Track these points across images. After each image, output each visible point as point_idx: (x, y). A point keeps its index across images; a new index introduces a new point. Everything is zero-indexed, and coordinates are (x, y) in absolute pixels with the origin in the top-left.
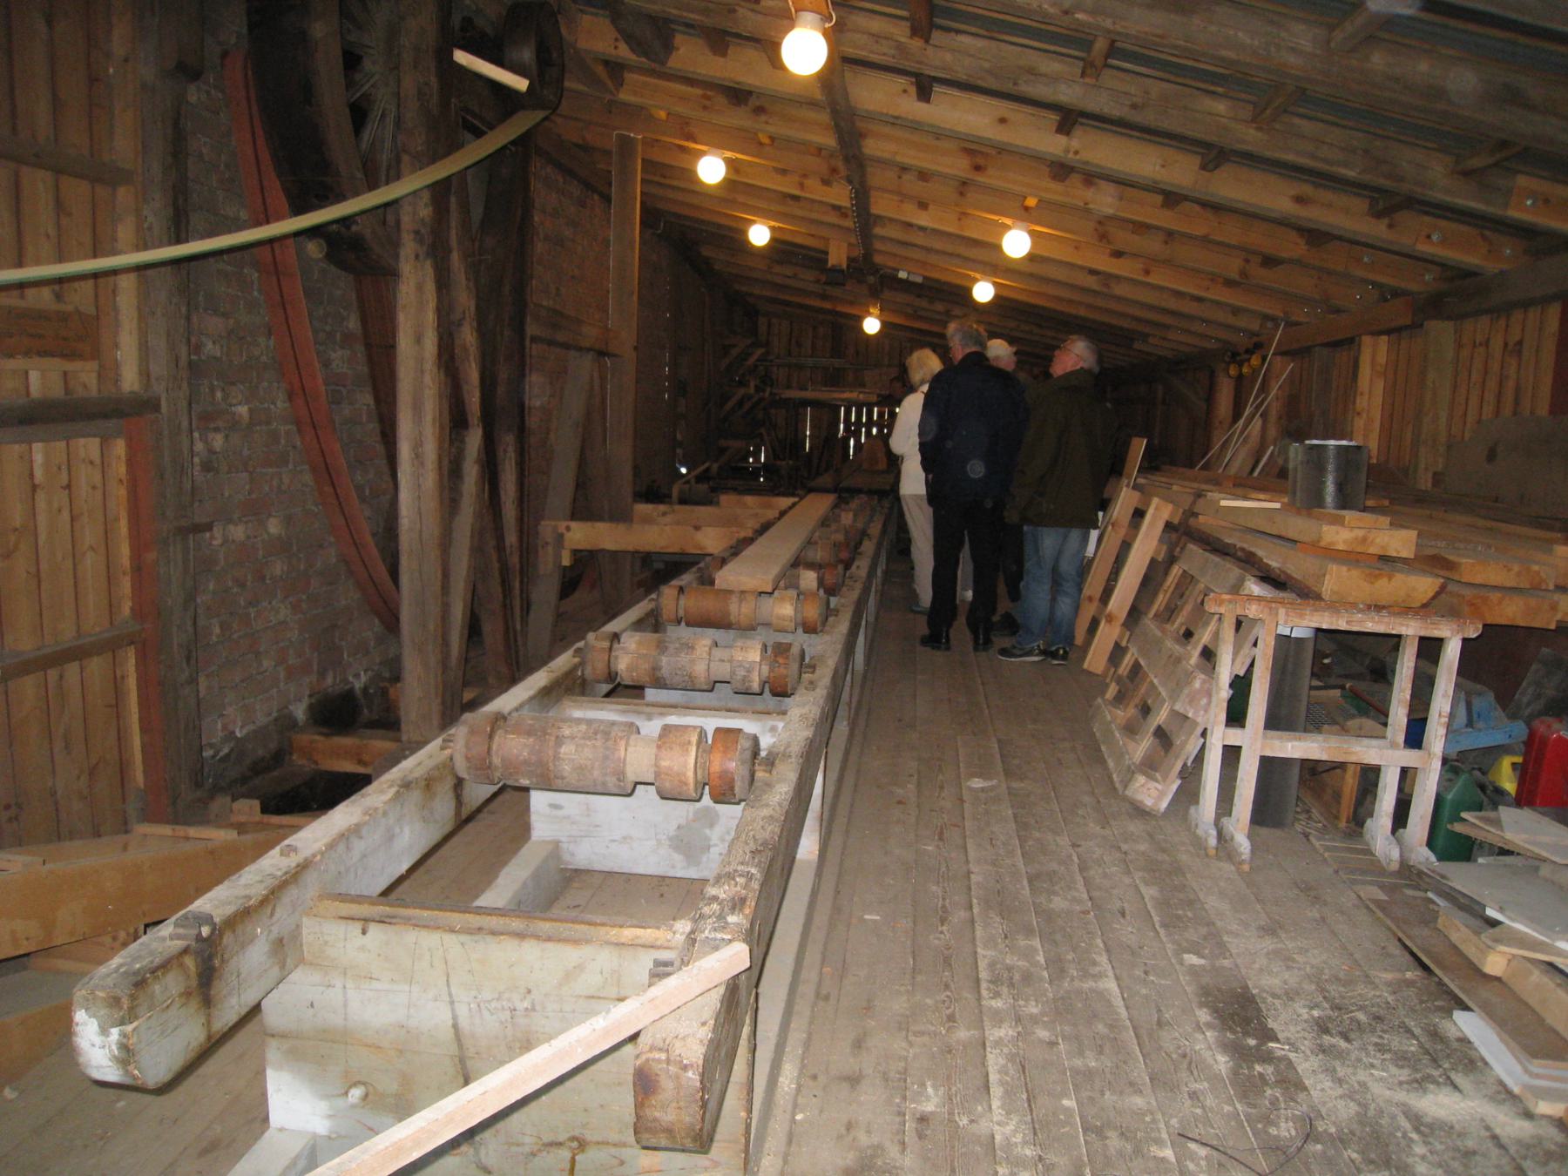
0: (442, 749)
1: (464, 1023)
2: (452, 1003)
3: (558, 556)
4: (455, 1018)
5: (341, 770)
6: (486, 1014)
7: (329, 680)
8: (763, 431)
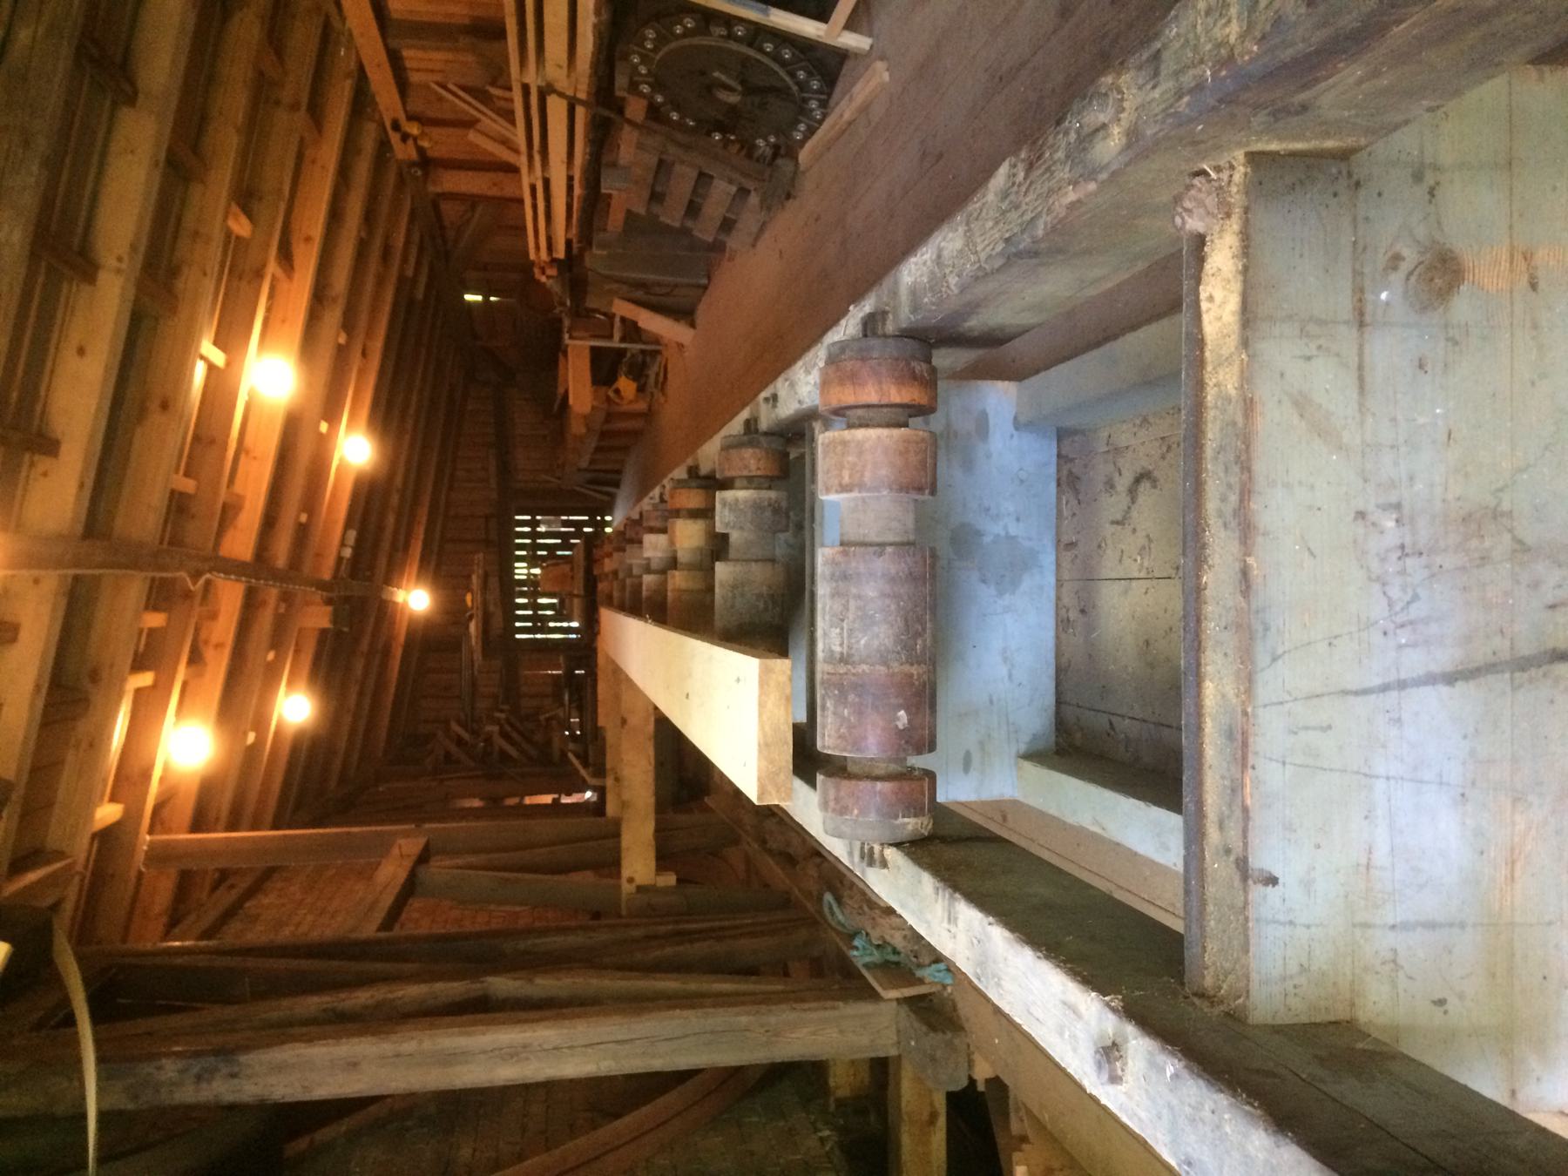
0: (884, 864)
1: (1445, 658)
2: (1402, 685)
3: (666, 891)
4: (1431, 679)
6: (1416, 611)
8: (542, 718)
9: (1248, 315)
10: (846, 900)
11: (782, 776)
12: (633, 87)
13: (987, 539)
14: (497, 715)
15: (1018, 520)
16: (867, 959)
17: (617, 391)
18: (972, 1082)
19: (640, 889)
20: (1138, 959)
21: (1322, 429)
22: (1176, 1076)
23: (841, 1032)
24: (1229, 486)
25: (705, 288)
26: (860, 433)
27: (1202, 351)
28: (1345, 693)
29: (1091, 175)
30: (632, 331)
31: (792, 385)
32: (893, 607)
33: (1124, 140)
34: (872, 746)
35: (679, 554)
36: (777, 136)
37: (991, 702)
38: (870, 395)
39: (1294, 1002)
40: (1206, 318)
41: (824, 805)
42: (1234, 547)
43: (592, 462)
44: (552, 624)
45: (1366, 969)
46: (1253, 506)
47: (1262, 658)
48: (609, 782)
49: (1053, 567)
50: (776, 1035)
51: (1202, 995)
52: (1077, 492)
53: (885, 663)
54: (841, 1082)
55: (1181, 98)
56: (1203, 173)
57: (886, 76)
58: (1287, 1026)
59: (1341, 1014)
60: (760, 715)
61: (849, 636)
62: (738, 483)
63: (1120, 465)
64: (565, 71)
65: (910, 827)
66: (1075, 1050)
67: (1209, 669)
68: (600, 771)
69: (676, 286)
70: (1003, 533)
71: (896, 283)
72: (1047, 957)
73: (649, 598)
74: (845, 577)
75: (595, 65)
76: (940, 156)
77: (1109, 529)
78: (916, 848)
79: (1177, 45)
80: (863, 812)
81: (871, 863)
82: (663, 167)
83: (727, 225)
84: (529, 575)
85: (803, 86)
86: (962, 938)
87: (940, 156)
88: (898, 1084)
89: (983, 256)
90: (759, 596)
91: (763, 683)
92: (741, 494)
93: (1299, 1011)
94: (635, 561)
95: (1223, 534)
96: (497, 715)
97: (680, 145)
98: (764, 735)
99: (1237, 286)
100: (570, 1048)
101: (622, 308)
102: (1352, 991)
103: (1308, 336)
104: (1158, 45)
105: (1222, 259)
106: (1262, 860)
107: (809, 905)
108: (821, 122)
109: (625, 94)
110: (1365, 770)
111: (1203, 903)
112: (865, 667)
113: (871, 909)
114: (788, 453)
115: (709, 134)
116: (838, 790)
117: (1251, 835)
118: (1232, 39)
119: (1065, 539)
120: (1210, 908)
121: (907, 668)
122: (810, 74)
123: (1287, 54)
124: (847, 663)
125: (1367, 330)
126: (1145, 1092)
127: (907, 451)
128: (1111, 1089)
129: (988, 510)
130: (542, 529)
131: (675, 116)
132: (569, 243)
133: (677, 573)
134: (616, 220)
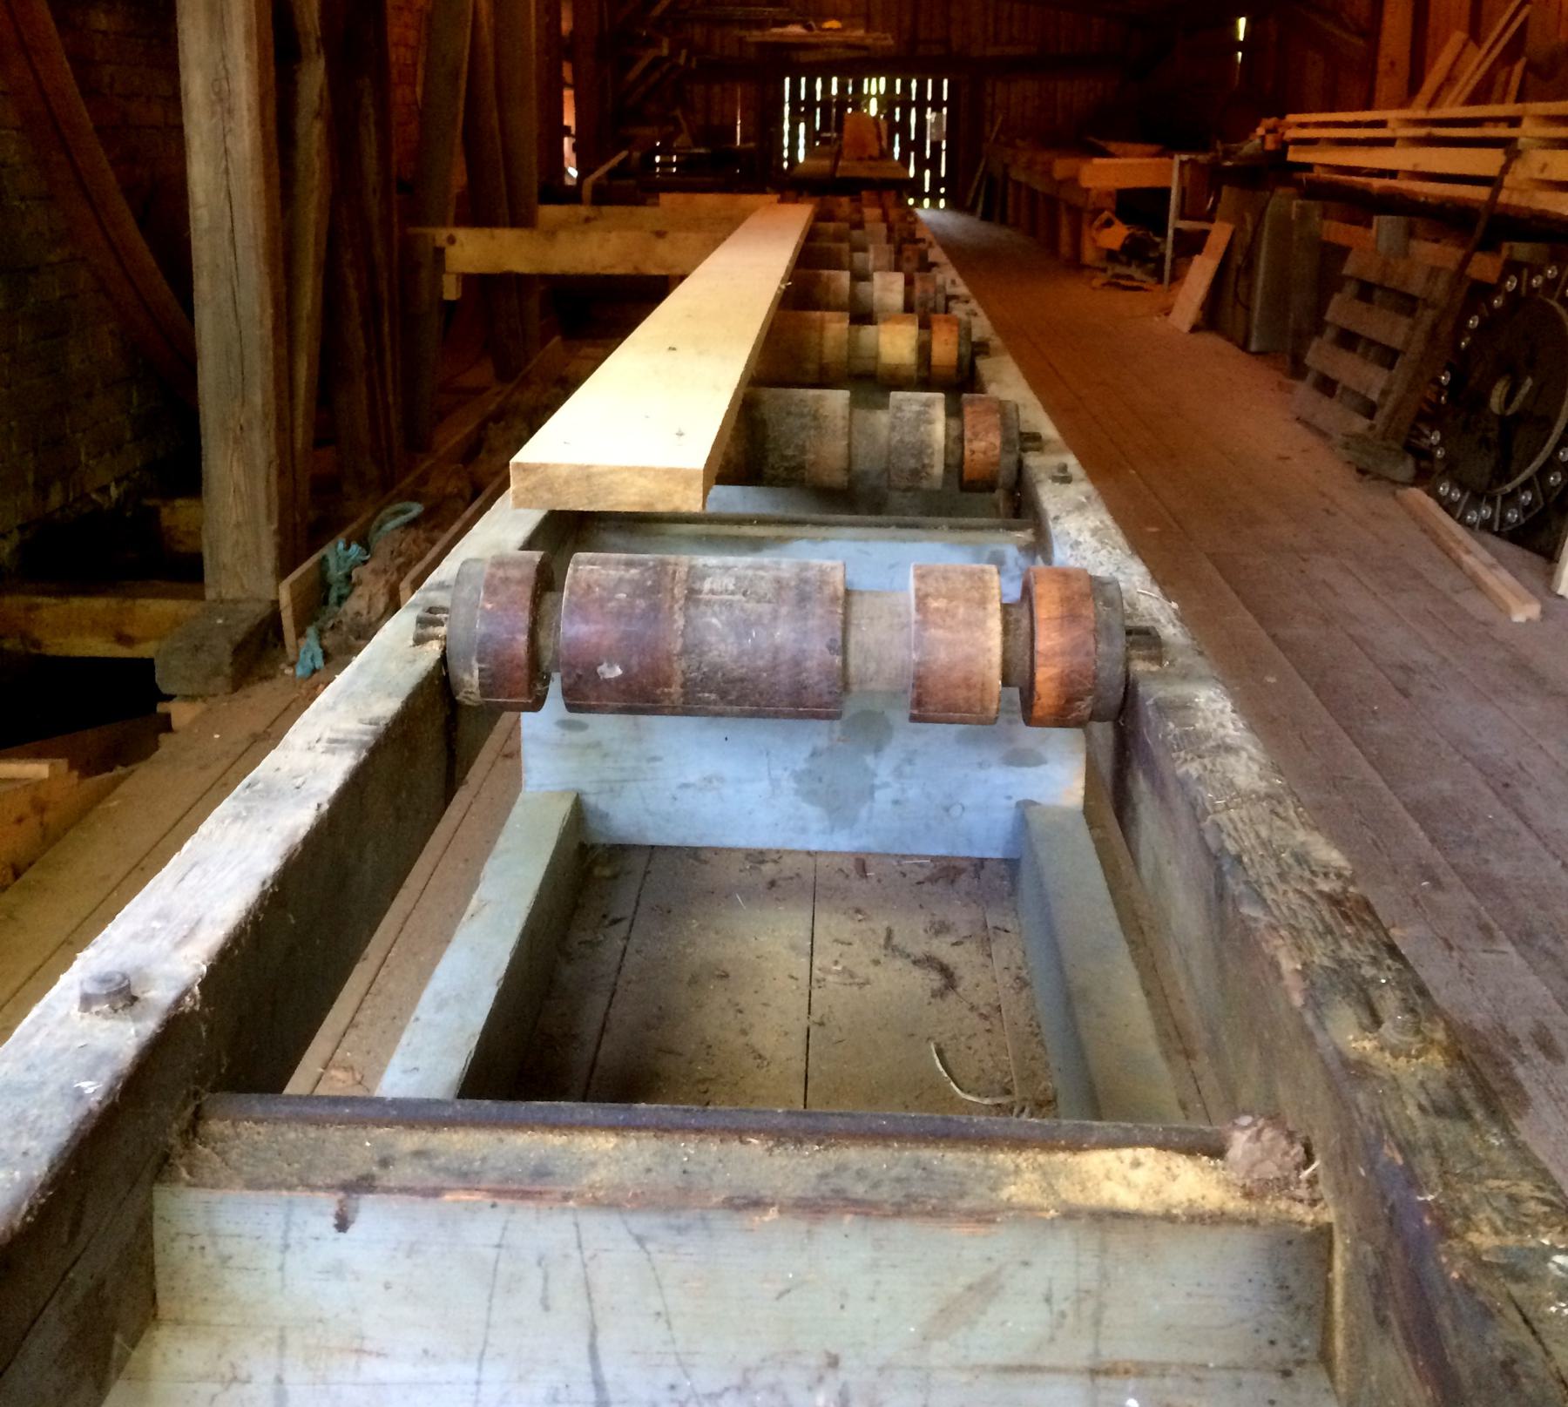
0: (420, 640)
3: (437, 286)
5: (79, 652)
7: (56, 499)
9: (1110, 1218)
10: (413, 533)
11: (547, 496)
12: (1512, 267)
13: (869, 760)
14: (684, 52)
15: (896, 802)
16: (332, 561)
17: (1108, 224)
18: (169, 698)
19: (440, 252)
20: (251, 1026)
21: (950, 1315)
22: (79, 1095)
23: (238, 525)
24: (876, 1185)
25: (1244, 347)
26: (995, 625)
27: (1064, 1149)
28: (594, 1332)
29: (1315, 1002)
30: (1191, 245)
31: (1080, 508)
32: (760, 663)
33: (1353, 1056)
34: (574, 628)
35: (870, 329)
36: (1444, 459)
37: (655, 759)
38: (1048, 640)
39: (182, 1244)
40: (1109, 1156)
41: (500, 563)
42: (794, 1189)
43: (1018, 184)
44: (802, 127)
45: (225, 1342)
46: (848, 1218)
47: (640, 1223)
48: (584, 210)
49: (831, 848)
50: (236, 441)
51: (198, 1116)
52: (932, 880)
53: (685, 651)
54: (176, 515)
55: (1401, 1149)
56: (1309, 1159)
57: (1519, 617)
58: (150, 1237)
59: (163, 1304)
60: (629, 469)
61: (722, 603)
62: (954, 423)
63: (967, 944)
64: (1537, 175)
65: (466, 677)
66: (135, 936)
67: (632, 1143)
68: (604, 196)
69: (1248, 309)
70: (877, 782)
71: (1201, 679)
72: (263, 895)
73: (818, 276)
74: (803, 599)
75: (1542, 217)
76: (1405, 694)
77: (880, 924)
78: (438, 687)
79: (1476, 1147)
80: (488, 614)
81: (422, 622)
82: (1407, 304)
83: (1327, 386)
84: (869, 96)
85: (1510, 499)
86: (307, 760)
87: (1405, 694)
88: (175, 596)
89: (1222, 818)
90: (803, 450)
91: (671, 473)
92: (938, 429)
93: (171, 1251)
94: (871, 256)
95: (812, 1172)
96: (684, 52)
97: (1435, 327)
98: (602, 474)
99: (1150, 1205)
100: (227, 171)
101: (1220, 234)
102: (195, 1323)
103: (1079, 1301)
104: (1479, 1115)
105: (1189, 1183)
106: (371, 1213)
107: (409, 480)
108: (1461, 520)
109: (1505, 253)
110: (489, 1353)
111: (319, 1123)
112: (681, 622)
113: (399, 569)
114: (998, 497)
115: (1449, 367)
116: (519, 582)
117: (405, 1198)
118: (1473, 1237)
119: (871, 862)
120: (313, 1132)
121: (678, 679)
122: (1527, 509)
123: (1444, 1319)
124: (687, 598)
125: (1086, 1380)
126: (69, 1044)
127: (969, 687)
128: (75, 994)
129: (910, 762)
130: (930, 116)
131: (1473, 322)
132: (1308, 167)
133: (846, 324)
134: (1336, 231)
